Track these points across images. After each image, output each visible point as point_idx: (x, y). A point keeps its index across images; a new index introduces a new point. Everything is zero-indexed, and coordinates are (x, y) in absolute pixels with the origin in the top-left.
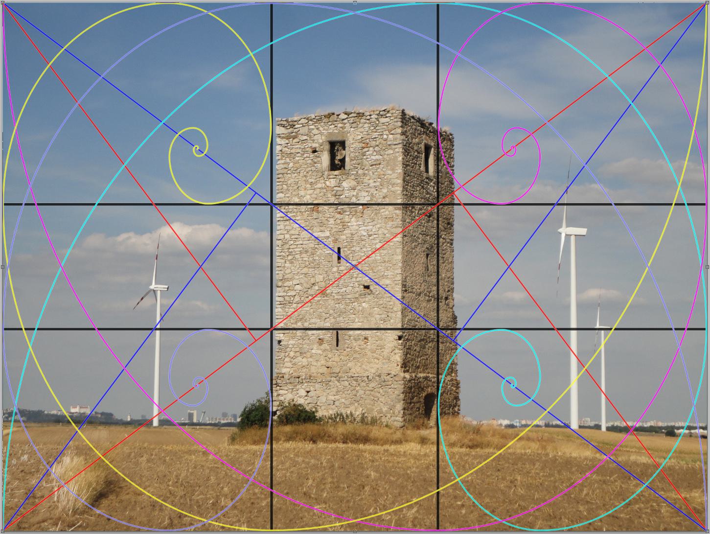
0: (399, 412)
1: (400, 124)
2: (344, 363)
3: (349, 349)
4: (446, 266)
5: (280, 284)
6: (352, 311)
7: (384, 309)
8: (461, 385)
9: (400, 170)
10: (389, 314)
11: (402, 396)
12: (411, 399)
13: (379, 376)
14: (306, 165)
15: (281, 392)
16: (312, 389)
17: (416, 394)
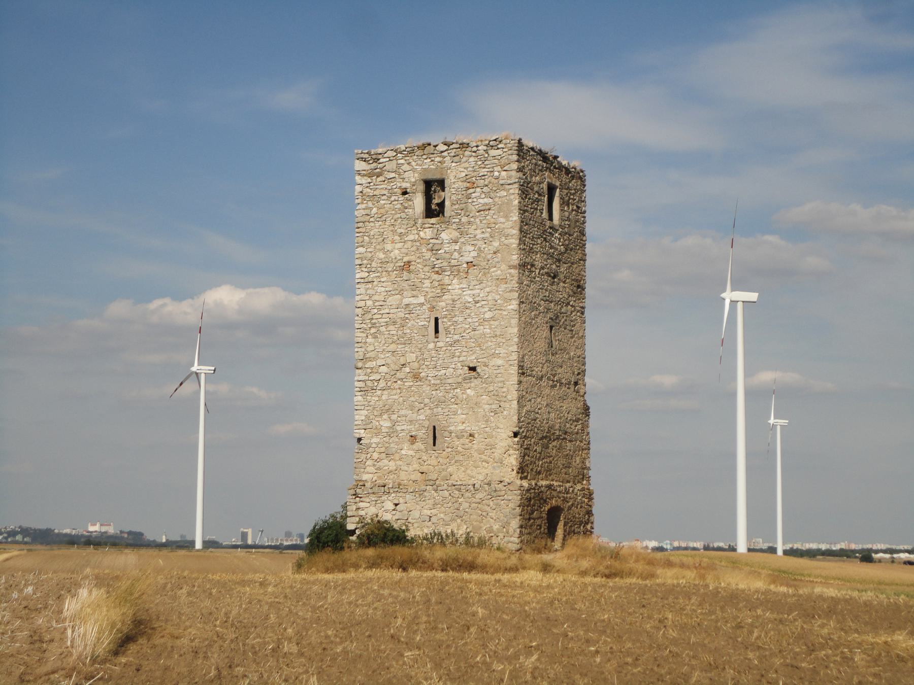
1: (515, 157)
5: (360, 365)
6: (453, 400)
8: (594, 496)
9: (515, 217)
10: (502, 404)
11: (518, 510)
12: (530, 514)
13: (489, 484)
15: (361, 505)
16: (401, 500)
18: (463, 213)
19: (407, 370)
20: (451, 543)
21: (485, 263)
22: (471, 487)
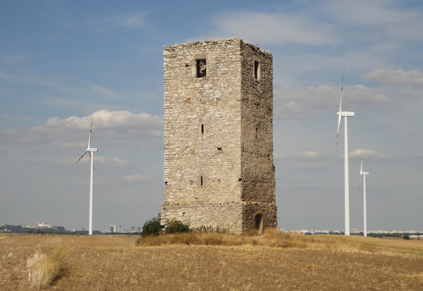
1: (239, 49)
3: (209, 187)
4: (268, 136)
5: (166, 147)
6: (210, 164)
8: (277, 209)
9: (239, 77)
10: (234, 165)
11: (242, 216)
12: (247, 218)
13: (228, 203)
15: (167, 213)
16: (186, 211)
18: (215, 75)
19: (189, 149)
21: (225, 99)
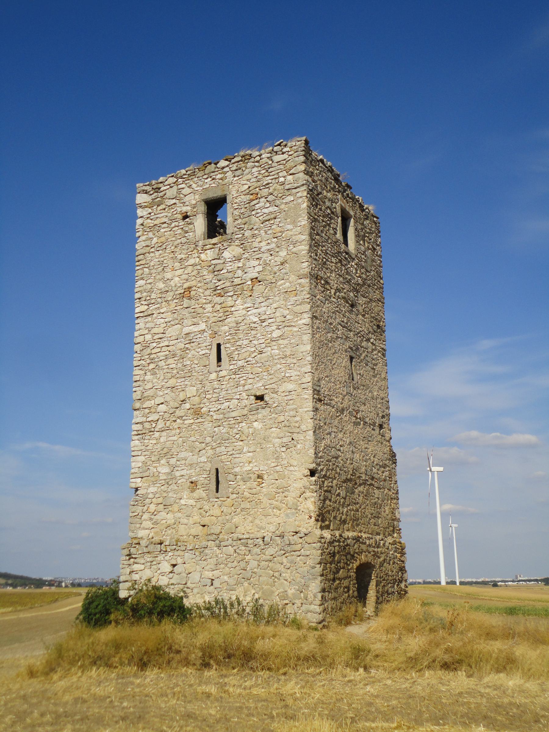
0: (315, 597)
1: (302, 159)
2: (227, 517)
3: (235, 496)
4: (377, 382)
5: (137, 405)
6: (238, 436)
7: (286, 429)
8: (406, 550)
9: (304, 221)
10: (295, 436)
11: (319, 569)
12: (335, 573)
13: (282, 536)
14: (174, 237)
15: (136, 567)
16: (179, 560)
17: (342, 565)
18: (246, 226)
19: (187, 406)
20: (237, 613)
21: (271, 277)
22: (260, 541)
